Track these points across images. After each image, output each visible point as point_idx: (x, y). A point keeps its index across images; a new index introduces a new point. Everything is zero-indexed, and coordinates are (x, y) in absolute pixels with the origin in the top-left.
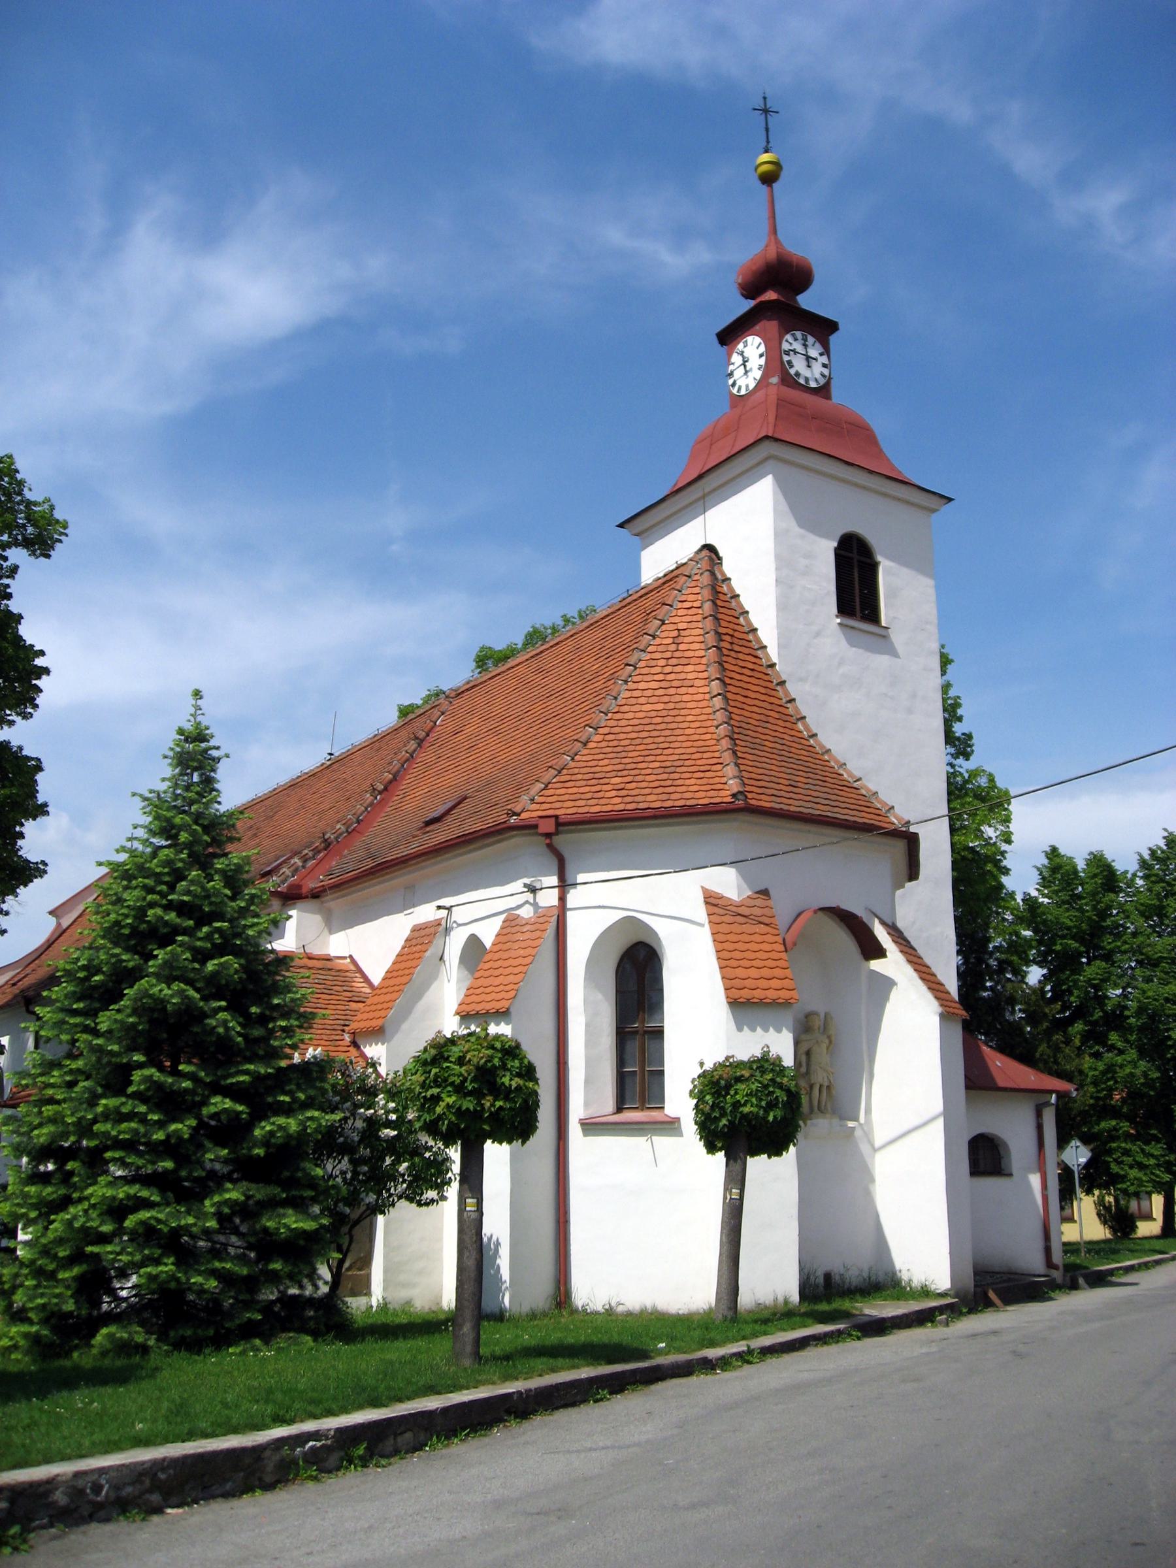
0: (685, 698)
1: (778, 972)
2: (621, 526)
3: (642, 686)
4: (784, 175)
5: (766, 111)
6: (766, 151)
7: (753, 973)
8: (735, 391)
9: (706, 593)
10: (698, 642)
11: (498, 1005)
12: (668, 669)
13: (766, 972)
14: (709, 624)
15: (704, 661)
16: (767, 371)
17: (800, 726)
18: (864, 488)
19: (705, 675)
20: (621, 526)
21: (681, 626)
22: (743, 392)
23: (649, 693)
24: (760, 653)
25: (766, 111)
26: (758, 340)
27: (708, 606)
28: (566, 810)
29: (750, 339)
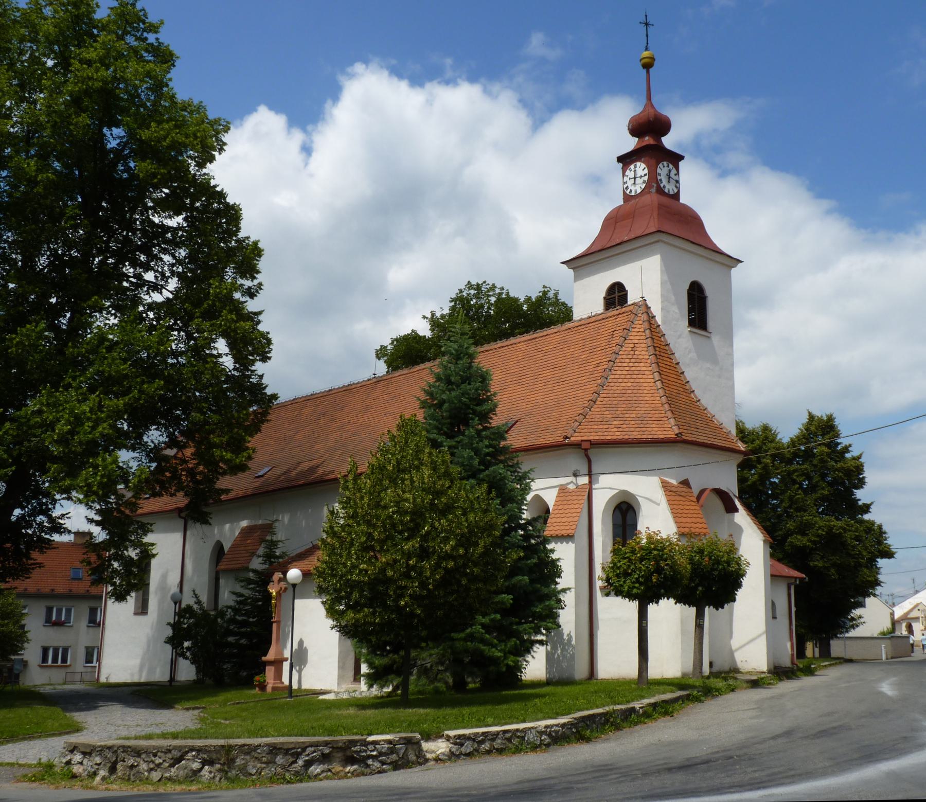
0: (642, 380)
1: (699, 520)
2: (563, 263)
3: (619, 372)
4: (656, 64)
5: (647, 24)
6: (647, 49)
7: (688, 520)
8: (628, 192)
9: (646, 325)
10: (644, 352)
11: (568, 532)
12: (631, 365)
13: (694, 520)
14: (649, 341)
15: (649, 361)
16: (648, 185)
17: (692, 395)
18: (702, 256)
19: (650, 369)
20: (563, 263)
21: (636, 341)
22: (633, 193)
23: (623, 377)
24: (672, 357)
25: (647, 24)
26: (643, 166)
27: (648, 332)
28: (594, 437)
29: (638, 164)
